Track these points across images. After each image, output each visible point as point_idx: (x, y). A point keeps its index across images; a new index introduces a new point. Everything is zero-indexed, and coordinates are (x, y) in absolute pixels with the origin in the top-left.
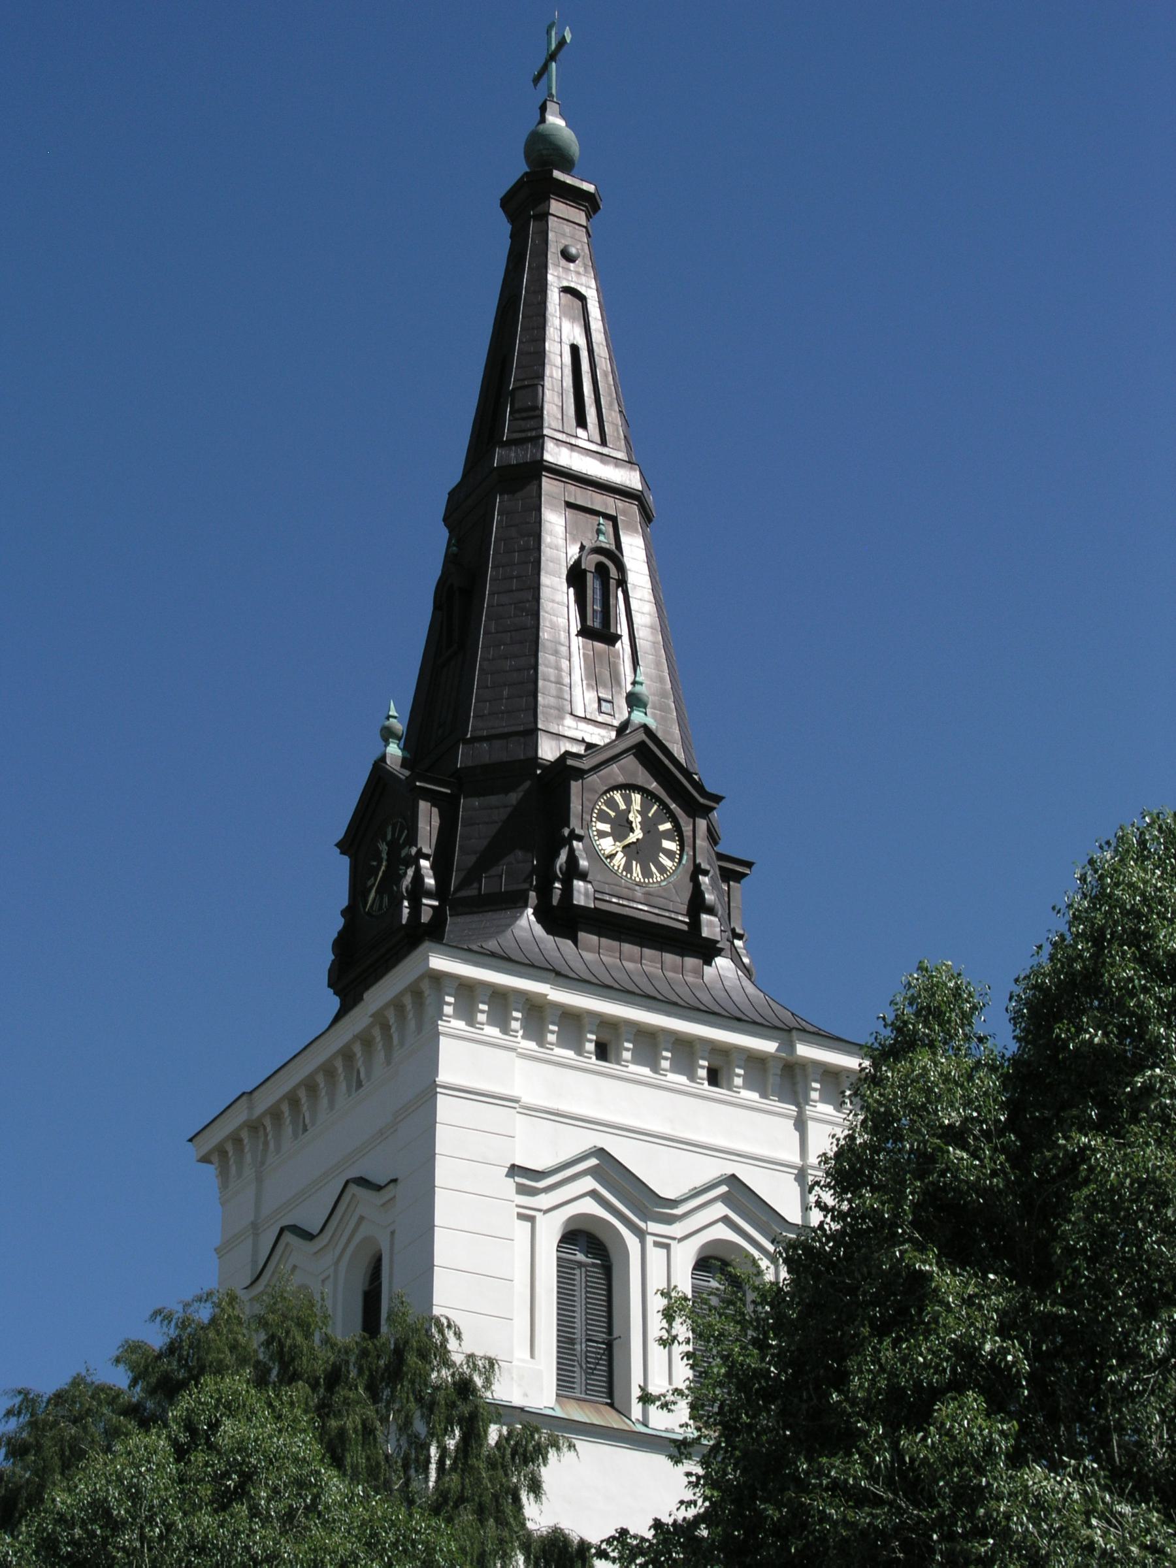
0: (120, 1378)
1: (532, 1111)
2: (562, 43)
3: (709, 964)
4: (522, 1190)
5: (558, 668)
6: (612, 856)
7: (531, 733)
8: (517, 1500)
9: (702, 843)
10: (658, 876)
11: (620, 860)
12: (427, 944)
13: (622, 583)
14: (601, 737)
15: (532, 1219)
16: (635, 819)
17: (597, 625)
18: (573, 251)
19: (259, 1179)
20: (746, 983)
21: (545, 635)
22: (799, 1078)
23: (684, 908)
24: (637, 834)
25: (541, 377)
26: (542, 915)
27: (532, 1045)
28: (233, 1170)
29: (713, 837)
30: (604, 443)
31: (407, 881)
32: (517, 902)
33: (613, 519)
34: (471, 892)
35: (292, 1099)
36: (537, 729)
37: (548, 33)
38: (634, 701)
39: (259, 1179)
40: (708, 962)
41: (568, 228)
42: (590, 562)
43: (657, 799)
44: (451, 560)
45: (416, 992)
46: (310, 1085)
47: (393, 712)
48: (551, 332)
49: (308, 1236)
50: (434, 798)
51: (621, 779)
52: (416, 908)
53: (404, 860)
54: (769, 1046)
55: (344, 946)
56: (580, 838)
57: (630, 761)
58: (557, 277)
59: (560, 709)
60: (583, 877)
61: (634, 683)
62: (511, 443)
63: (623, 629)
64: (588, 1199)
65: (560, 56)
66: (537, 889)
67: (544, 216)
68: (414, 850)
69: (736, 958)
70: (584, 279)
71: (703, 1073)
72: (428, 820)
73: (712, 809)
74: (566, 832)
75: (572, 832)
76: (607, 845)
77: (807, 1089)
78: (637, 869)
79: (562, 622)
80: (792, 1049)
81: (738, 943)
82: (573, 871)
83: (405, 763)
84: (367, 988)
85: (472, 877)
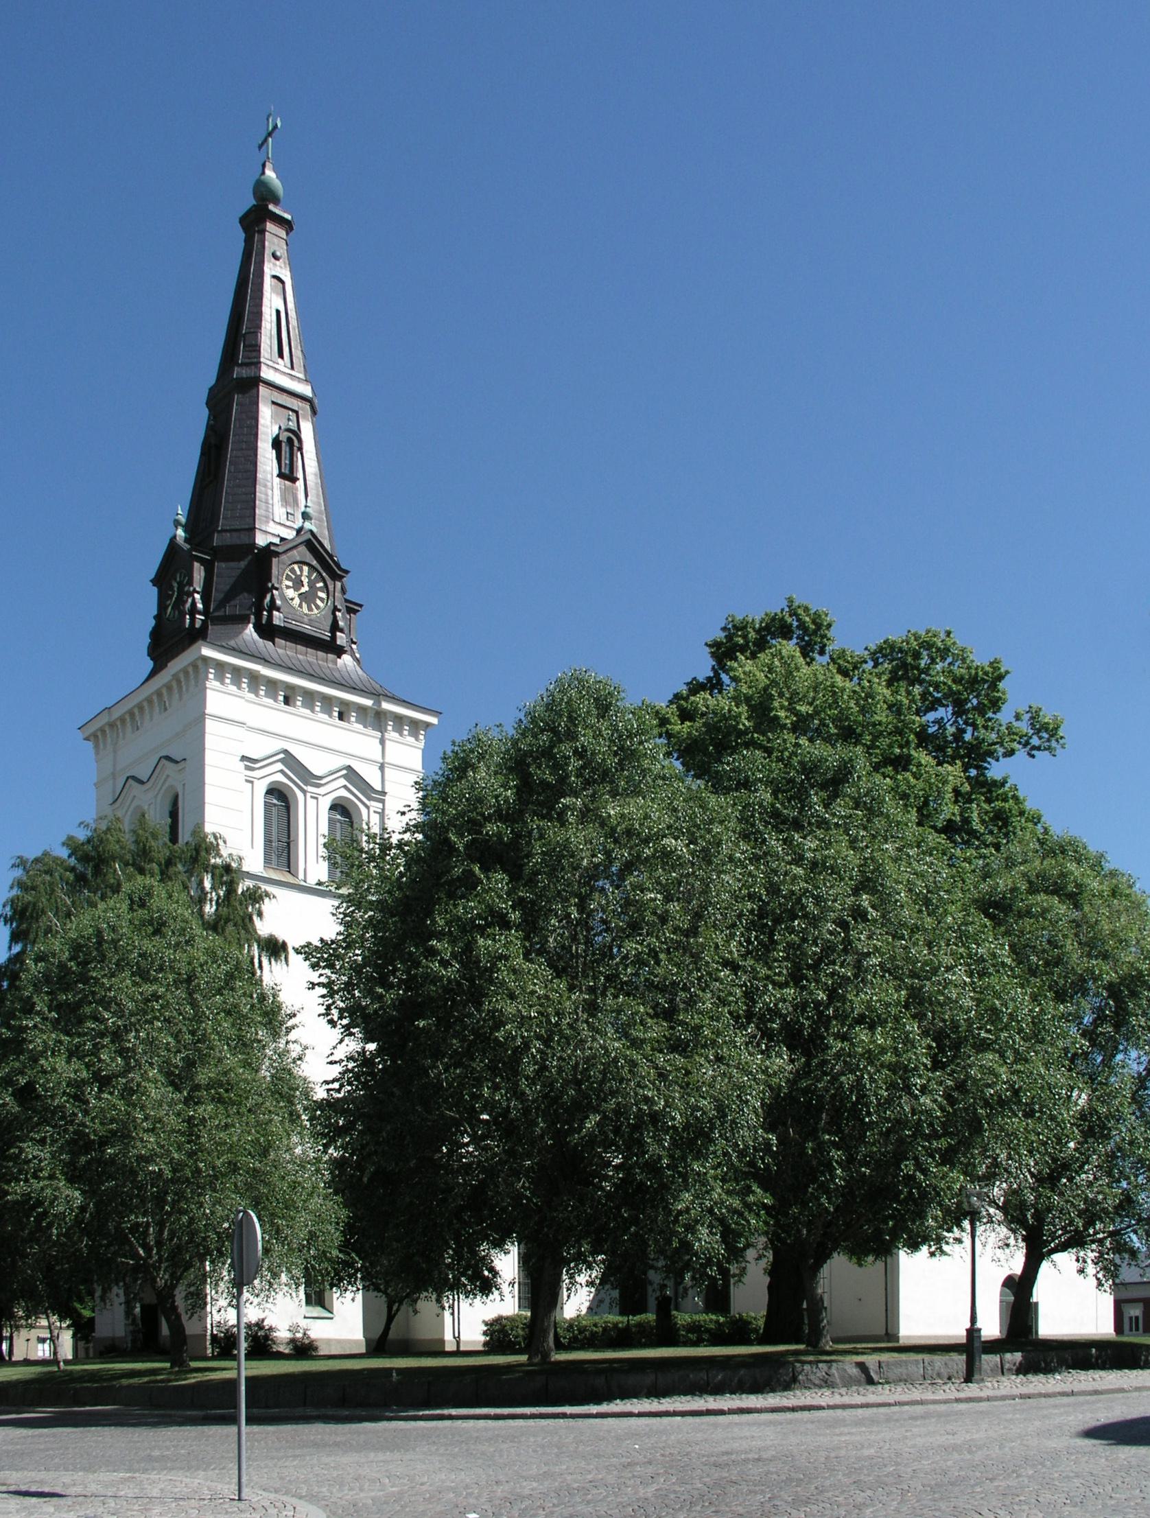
0: (63, 853)
1: (251, 728)
2: (275, 127)
3: (339, 657)
4: (248, 768)
5: (267, 495)
6: (292, 599)
7: (252, 530)
8: (251, 919)
9: (338, 594)
10: (316, 611)
11: (297, 601)
12: (200, 642)
13: (300, 449)
14: (290, 534)
15: (252, 782)
16: (305, 581)
17: (287, 472)
18: (278, 254)
19: (115, 751)
20: (358, 669)
21: (259, 475)
22: (383, 719)
23: (328, 628)
24: (305, 589)
25: (260, 327)
26: (259, 629)
27: (252, 696)
28: (101, 746)
29: (343, 591)
30: (292, 368)
31: (188, 605)
32: (244, 620)
33: (296, 412)
34: (220, 613)
35: (131, 713)
36: (255, 528)
37: (268, 119)
38: (305, 516)
39: (115, 751)
40: (339, 657)
41: (276, 240)
42: (283, 437)
43: (316, 570)
44: (211, 429)
45: (195, 666)
46: (140, 707)
47: (180, 512)
48: (266, 301)
49: (141, 782)
50: (201, 561)
51: (298, 559)
52: (193, 619)
53: (184, 594)
54: (368, 702)
55: (156, 635)
56: (277, 589)
57: (303, 549)
58: (270, 268)
59: (267, 517)
60: (278, 609)
61: (306, 506)
62: (243, 364)
63: (300, 475)
64: (279, 774)
65: (274, 135)
66: (254, 614)
67: (263, 232)
68: (191, 589)
69: (353, 656)
70: (284, 271)
71: (336, 714)
72: (199, 573)
73: (343, 577)
74: (270, 585)
75: (273, 585)
76: (290, 593)
77: (387, 725)
78: (305, 605)
79: (269, 469)
80: (380, 705)
81: (354, 646)
82: (273, 606)
83: (186, 540)
84: (169, 661)
85: (221, 604)
